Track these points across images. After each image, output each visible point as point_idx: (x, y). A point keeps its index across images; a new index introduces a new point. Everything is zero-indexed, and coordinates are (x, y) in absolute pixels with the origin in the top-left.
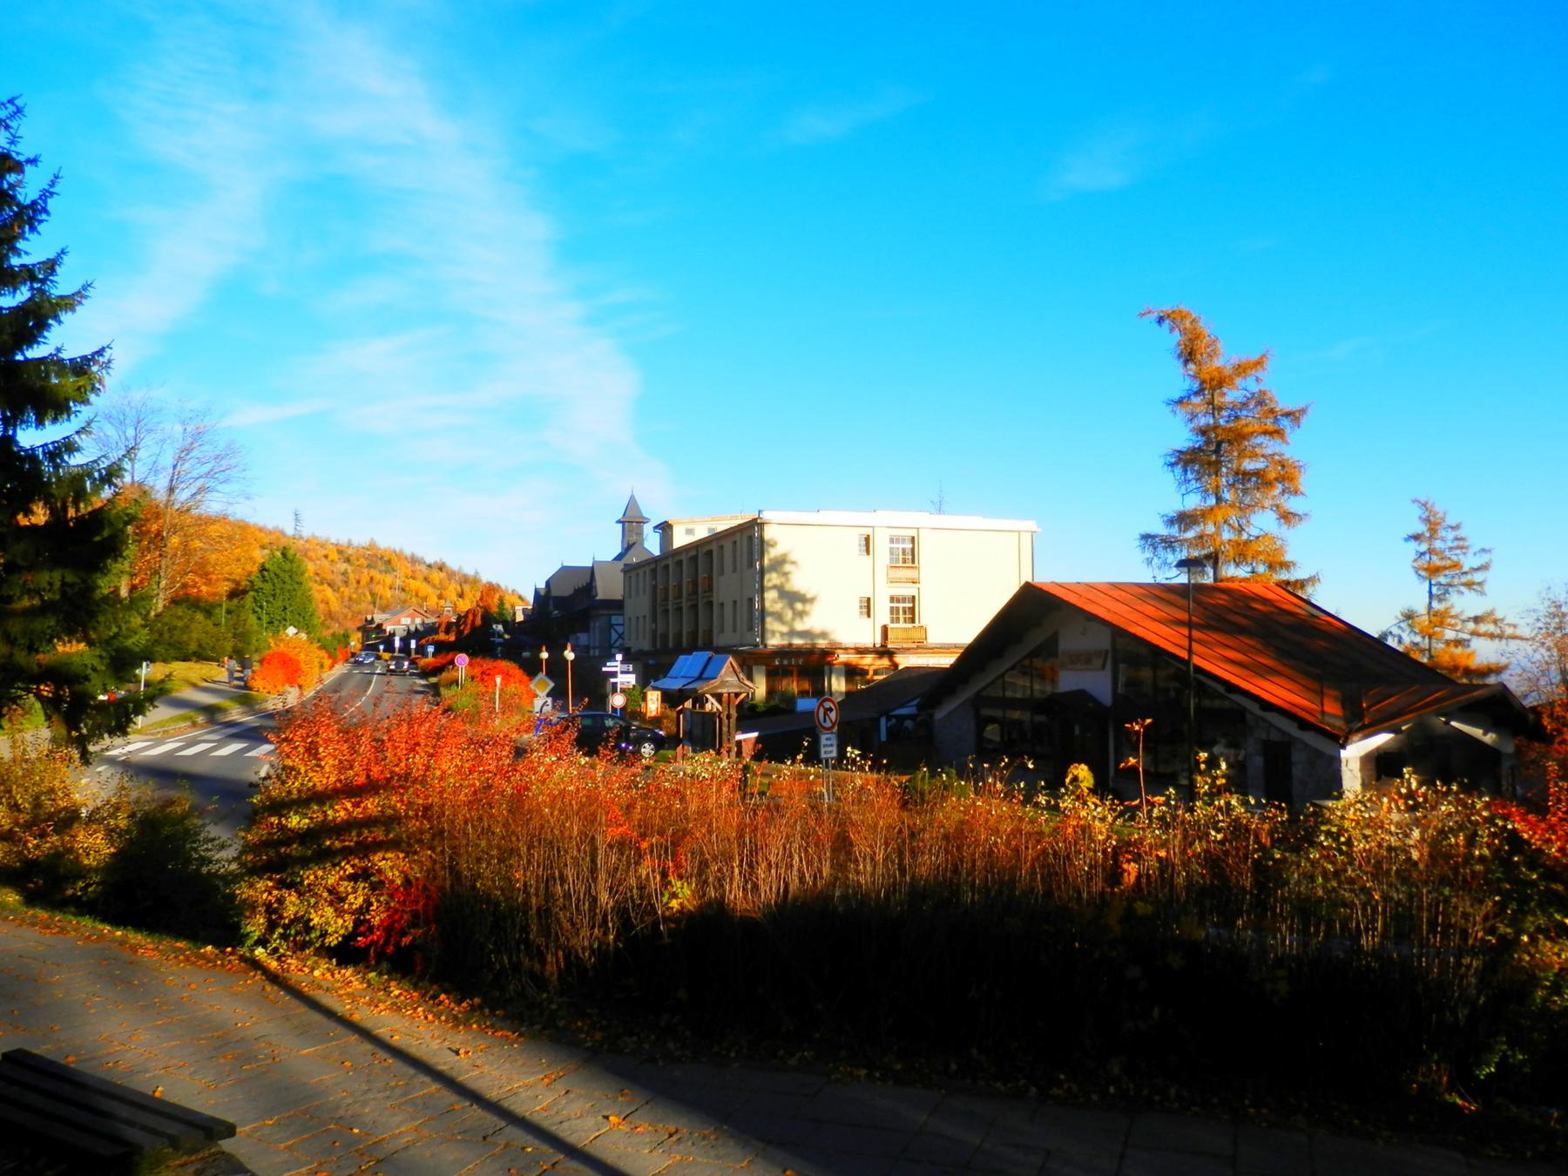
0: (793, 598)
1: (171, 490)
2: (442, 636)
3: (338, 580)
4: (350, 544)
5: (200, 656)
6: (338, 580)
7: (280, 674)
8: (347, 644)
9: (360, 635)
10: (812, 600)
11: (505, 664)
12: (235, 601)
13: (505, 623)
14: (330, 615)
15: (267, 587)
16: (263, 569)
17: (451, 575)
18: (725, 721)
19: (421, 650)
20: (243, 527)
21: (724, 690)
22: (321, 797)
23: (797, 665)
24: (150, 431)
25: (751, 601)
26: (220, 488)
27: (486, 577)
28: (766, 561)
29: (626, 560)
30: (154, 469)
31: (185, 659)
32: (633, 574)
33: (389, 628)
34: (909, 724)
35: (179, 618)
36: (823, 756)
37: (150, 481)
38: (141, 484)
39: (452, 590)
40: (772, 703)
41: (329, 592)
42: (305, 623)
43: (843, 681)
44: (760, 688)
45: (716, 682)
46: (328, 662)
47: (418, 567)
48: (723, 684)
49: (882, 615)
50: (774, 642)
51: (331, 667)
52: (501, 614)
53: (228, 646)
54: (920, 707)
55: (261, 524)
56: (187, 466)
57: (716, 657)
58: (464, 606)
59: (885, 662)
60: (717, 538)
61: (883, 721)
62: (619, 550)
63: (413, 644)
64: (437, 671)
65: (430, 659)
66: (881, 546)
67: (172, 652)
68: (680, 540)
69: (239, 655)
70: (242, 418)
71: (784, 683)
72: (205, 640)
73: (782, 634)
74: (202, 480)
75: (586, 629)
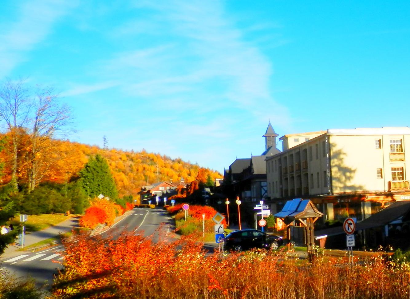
0: (345, 170)
1: (36, 130)
2: (179, 195)
3: (128, 170)
4: (133, 151)
5: (55, 211)
6: (128, 170)
7: (95, 218)
8: (131, 201)
9: (139, 196)
10: (354, 171)
11: (209, 208)
12: (72, 183)
13: (211, 188)
14: (125, 187)
15: (90, 175)
16: (87, 166)
17: (184, 165)
18: (309, 231)
19: (169, 203)
20: (77, 145)
21: (307, 216)
22: (80, 279)
23: (348, 202)
24: (23, 101)
25: (325, 172)
26: (61, 127)
27: (202, 165)
28: (331, 154)
29: (267, 155)
30: (26, 120)
31: (48, 212)
32: (270, 162)
33: (153, 192)
34: (399, 228)
35: (43, 193)
36: (348, 245)
37: (24, 125)
38: (20, 127)
39: (185, 173)
40: (337, 221)
41: (123, 176)
42: (108, 191)
43: (370, 209)
44: (331, 214)
45: (303, 213)
46: (121, 211)
47: (167, 162)
48: (307, 213)
49: (388, 177)
50: (337, 192)
51: (123, 213)
52: (209, 183)
53: (69, 205)
54: (403, 220)
55: (87, 143)
56: (43, 118)
57: (303, 200)
58: (192, 179)
59: (390, 199)
60: (309, 143)
61: (386, 227)
62: (264, 150)
63: (165, 200)
64: (175, 212)
65: (173, 207)
66: (386, 144)
67: (40, 210)
68: (292, 144)
69: (75, 210)
70: (70, 91)
71: (342, 211)
72: (57, 203)
73: (341, 188)
74: (51, 124)
75: (249, 189)
